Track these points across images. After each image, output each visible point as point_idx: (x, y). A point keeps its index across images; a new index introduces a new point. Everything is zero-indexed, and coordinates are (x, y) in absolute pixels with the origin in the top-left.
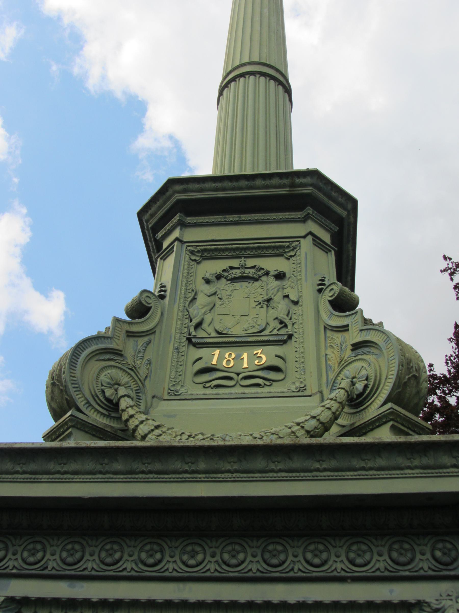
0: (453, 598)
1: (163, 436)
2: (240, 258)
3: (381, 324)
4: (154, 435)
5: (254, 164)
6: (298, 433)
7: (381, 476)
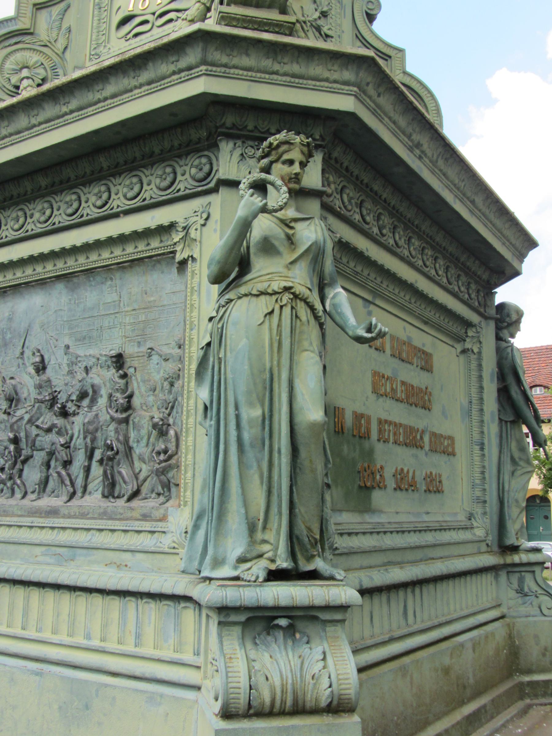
0: (199, 214)
7: (116, 104)
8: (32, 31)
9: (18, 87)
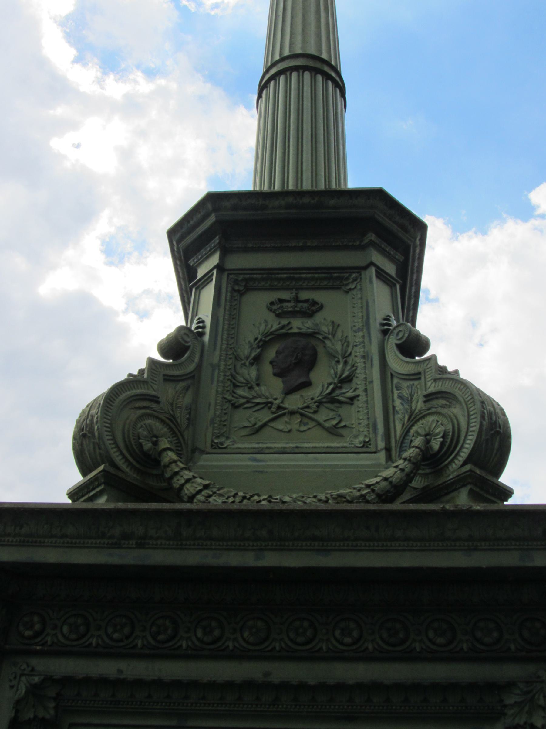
1: (213, 497)
2: (291, 289)
3: (456, 372)
4: (203, 495)
5: (284, 180)
6: (369, 496)
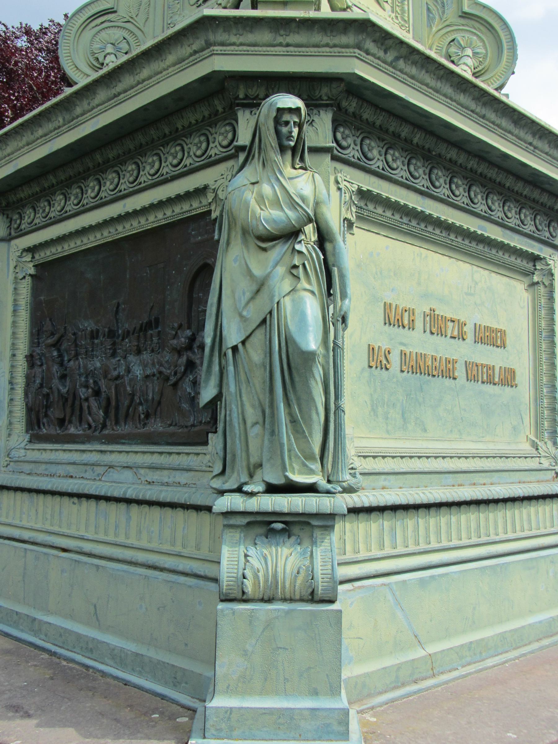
8: (115, 9)
9: (102, 64)
